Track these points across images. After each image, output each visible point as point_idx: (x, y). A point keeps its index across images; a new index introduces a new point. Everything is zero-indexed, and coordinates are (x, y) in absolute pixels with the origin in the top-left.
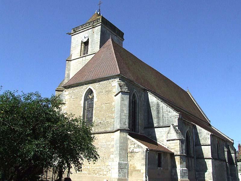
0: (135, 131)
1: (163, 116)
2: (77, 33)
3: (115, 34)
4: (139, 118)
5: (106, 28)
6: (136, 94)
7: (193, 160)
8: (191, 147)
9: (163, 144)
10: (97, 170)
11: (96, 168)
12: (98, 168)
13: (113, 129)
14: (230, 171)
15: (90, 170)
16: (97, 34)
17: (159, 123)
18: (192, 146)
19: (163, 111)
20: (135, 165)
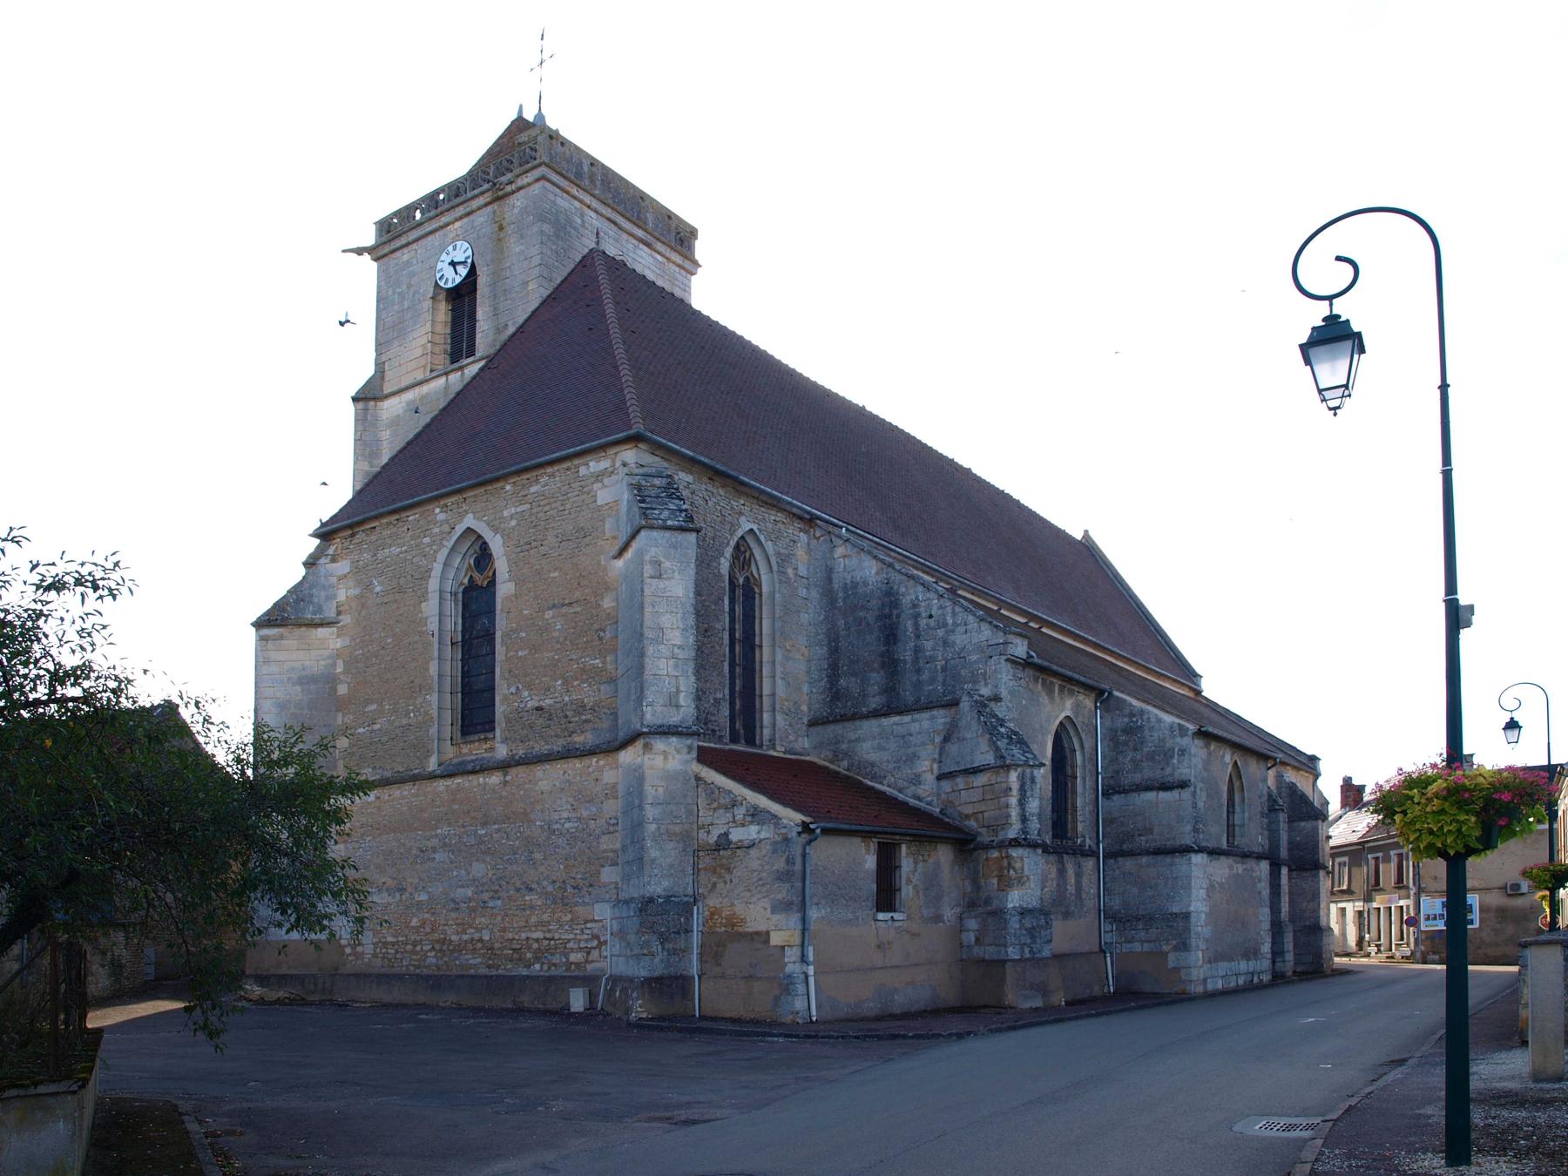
0: (751, 741)
1: (917, 651)
2: (403, 240)
3: (640, 233)
4: (778, 674)
5: (575, 198)
6: (752, 544)
7: (1089, 864)
8: (1079, 801)
9: (919, 799)
10: (535, 946)
11: (524, 936)
12: (539, 935)
13: (608, 737)
14: (1291, 902)
15: (497, 945)
16: (522, 237)
17: (893, 689)
18: (1090, 796)
19: (916, 626)
20: (739, 909)
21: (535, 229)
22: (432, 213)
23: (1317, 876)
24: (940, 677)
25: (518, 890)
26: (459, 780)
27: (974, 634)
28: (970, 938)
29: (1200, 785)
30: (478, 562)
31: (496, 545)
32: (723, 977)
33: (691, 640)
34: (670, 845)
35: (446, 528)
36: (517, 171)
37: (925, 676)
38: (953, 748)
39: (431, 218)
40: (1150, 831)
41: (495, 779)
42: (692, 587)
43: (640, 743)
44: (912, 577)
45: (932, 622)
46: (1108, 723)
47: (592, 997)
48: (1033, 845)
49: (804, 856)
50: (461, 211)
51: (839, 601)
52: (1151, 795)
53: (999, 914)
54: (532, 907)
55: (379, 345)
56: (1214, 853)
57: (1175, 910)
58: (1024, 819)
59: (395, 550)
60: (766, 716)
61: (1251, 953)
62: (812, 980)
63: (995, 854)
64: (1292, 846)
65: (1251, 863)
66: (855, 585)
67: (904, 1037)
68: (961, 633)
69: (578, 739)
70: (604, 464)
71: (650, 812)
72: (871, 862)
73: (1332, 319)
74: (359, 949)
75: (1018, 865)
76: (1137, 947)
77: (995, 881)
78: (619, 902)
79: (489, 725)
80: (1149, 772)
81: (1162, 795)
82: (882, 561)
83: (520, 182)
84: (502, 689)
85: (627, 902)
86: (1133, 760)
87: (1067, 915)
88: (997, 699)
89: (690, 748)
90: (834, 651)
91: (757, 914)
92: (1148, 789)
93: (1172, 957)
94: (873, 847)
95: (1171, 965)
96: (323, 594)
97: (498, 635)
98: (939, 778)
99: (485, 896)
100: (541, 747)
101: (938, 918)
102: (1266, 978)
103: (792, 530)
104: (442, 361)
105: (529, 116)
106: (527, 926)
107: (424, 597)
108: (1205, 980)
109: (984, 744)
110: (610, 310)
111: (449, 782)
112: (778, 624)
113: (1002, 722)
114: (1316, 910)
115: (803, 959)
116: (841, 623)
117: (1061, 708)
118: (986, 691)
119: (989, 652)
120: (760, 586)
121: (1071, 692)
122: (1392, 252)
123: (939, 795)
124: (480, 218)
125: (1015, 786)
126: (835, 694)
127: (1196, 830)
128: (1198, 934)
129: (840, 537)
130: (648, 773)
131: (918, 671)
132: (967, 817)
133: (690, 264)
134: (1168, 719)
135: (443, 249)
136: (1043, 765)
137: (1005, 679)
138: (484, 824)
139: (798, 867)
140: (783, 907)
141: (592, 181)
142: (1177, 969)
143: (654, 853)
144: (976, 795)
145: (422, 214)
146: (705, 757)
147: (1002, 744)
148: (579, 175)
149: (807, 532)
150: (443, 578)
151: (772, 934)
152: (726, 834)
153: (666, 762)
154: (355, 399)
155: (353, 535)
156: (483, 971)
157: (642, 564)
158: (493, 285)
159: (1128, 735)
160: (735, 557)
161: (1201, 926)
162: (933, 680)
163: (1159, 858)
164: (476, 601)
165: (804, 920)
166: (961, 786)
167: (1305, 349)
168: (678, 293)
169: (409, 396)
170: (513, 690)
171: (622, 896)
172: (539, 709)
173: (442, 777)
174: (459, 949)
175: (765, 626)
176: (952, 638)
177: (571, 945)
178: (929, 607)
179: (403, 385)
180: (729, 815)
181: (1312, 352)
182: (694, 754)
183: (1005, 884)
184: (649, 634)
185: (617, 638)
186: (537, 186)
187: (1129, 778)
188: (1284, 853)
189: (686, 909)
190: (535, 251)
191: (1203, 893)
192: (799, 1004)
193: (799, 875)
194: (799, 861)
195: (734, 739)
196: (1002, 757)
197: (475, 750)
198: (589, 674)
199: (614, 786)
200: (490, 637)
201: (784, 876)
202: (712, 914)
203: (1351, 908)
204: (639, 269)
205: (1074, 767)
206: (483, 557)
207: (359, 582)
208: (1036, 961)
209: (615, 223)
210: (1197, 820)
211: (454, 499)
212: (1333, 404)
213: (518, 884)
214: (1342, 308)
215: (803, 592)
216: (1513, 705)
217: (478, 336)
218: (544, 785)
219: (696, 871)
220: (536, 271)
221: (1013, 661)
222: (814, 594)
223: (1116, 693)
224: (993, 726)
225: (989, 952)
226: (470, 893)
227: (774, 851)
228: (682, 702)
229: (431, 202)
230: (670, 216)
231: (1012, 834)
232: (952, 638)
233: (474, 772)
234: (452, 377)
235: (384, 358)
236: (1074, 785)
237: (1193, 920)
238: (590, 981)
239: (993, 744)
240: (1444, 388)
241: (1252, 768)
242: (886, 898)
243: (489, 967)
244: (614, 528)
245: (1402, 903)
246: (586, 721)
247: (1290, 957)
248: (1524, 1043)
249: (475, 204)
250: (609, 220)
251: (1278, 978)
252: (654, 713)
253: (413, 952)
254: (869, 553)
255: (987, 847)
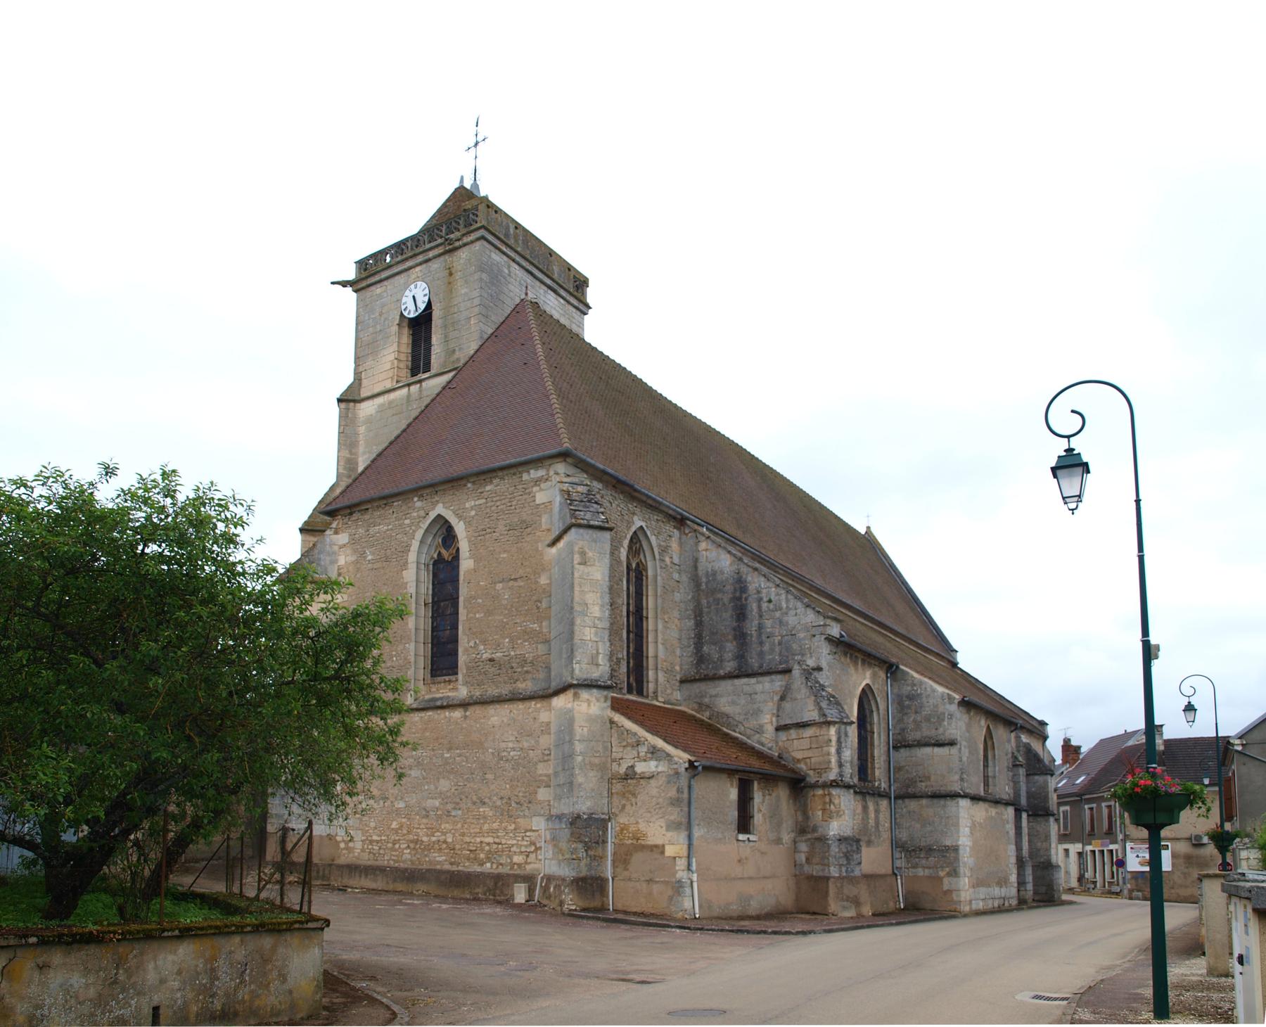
0: (640, 692)
1: (760, 627)
2: (377, 278)
4: (660, 640)
10: (487, 848)
11: (478, 840)
12: (490, 840)
13: (544, 685)
14: (1030, 841)
15: (458, 847)
19: (760, 607)
20: (642, 826)
21: (476, 276)
22: (400, 258)
23: (1047, 821)
24: (777, 649)
25: (474, 803)
26: (430, 713)
27: (801, 617)
28: (802, 858)
29: (964, 743)
30: (444, 541)
31: (460, 529)
32: (630, 879)
33: (607, 613)
34: (591, 774)
35: (422, 513)
36: (464, 231)
37: (766, 648)
38: (787, 705)
39: (398, 263)
40: (928, 778)
41: (457, 714)
42: (607, 572)
43: (570, 693)
44: (756, 569)
45: (771, 606)
46: (896, 691)
47: (531, 891)
48: (848, 787)
49: (690, 787)
50: (420, 258)
51: (702, 586)
52: (928, 750)
53: (823, 839)
54: (485, 818)
55: (357, 359)
56: (975, 798)
57: (948, 843)
58: (841, 765)
59: (383, 528)
60: (651, 673)
61: (1003, 882)
62: (695, 885)
63: (820, 792)
64: (1030, 796)
65: (1001, 808)
66: (714, 573)
67: (765, 932)
68: (795, 621)
69: (521, 686)
70: (541, 473)
71: (579, 747)
72: (733, 794)
73: (1069, 450)
74: (351, 844)
75: (836, 802)
76: (920, 872)
77: (820, 813)
78: (550, 818)
79: (453, 669)
80: (927, 732)
81: (936, 750)
82: (734, 555)
83: (466, 240)
84: (465, 643)
85: (560, 817)
86: (914, 721)
87: (869, 843)
88: (819, 669)
89: (606, 698)
90: (699, 624)
91: (656, 831)
92: (927, 745)
93: (946, 881)
94: (736, 783)
95: (946, 887)
96: (328, 558)
97: (461, 599)
98: (778, 729)
99: (449, 807)
100: (493, 691)
101: (778, 841)
102: (1014, 902)
103: (669, 528)
104: (405, 373)
105: (468, 185)
106: (481, 833)
107: (405, 566)
108: (971, 901)
109: (810, 704)
110: (539, 348)
111: (422, 714)
112: (659, 601)
113: (823, 688)
114: (1048, 849)
115: (689, 868)
116: (704, 602)
117: (863, 678)
118: (811, 662)
119: (814, 631)
120: (646, 570)
121: (870, 665)
122: (1104, 410)
123: (777, 742)
124: (435, 265)
125: (834, 739)
126: (700, 659)
127: (962, 779)
128: (965, 863)
129: (703, 534)
130: (576, 715)
131: (761, 643)
132: (799, 761)
133: (583, 307)
134: (940, 689)
135: (406, 286)
136: (852, 723)
137: (823, 655)
138: (449, 749)
139: (686, 795)
140: (673, 826)
141: (516, 241)
142: (949, 892)
143: (580, 779)
144: (805, 744)
145: (392, 257)
146: (617, 706)
147: (824, 704)
148: (507, 235)
149: (679, 529)
150: (419, 552)
151: (667, 847)
152: (632, 767)
153: (588, 709)
154: (339, 401)
155: (351, 514)
156: (447, 867)
157: (572, 553)
158: (445, 317)
159: (907, 703)
160: (630, 547)
161: (967, 857)
162: (772, 650)
163: (935, 801)
164: (444, 574)
165: (690, 837)
166: (794, 736)
167: (1054, 470)
168: (575, 329)
169: (380, 400)
170: (472, 644)
171: (554, 812)
172: (491, 660)
173: (417, 710)
174: (429, 848)
175: (650, 603)
176: (785, 619)
177: (514, 849)
178: (768, 593)
179: (376, 391)
180: (635, 752)
181: (1059, 473)
182: (609, 703)
183: (828, 815)
184: (577, 608)
185: (547, 607)
186: (478, 244)
187: (913, 736)
188: (1024, 801)
189: (603, 824)
190: (476, 293)
191: (967, 830)
192: (687, 904)
193: (686, 801)
194: (686, 791)
195: (630, 691)
196: (824, 715)
197: (443, 692)
198: (529, 635)
199: (548, 724)
200: (454, 600)
201: (675, 802)
202: (622, 830)
203: (1075, 848)
204: (548, 310)
205: (872, 724)
206: (448, 535)
207: (355, 551)
208: (852, 880)
209: (532, 274)
210: (962, 771)
211: (428, 491)
212: (1073, 506)
213: (474, 798)
214: (1075, 443)
215: (676, 576)
216: (1189, 692)
217: (433, 357)
218: (495, 720)
219: (610, 794)
220: (476, 310)
221: (830, 639)
222: (685, 578)
223: (902, 667)
224: (817, 690)
225: (816, 870)
226: (437, 803)
227: (669, 782)
228: (600, 662)
229: (399, 248)
230: (570, 268)
231: (832, 775)
232: (785, 619)
233: (442, 707)
234: (413, 388)
235: (361, 369)
236: (872, 738)
237: (961, 852)
238: (529, 879)
239: (818, 704)
240: (1138, 501)
241: (1000, 733)
242: (744, 824)
243: (452, 864)
244: (551, 522)
245: (1112, 847)
246: (527, 672)
247: (1030, 887)
248: (1204, 954)
249: (431, 254)
250: (527, 271)
251: (1022, 904)
252: (581, 670)
253: (393, 849)
254: (725, 548)
255: (815, 786)
